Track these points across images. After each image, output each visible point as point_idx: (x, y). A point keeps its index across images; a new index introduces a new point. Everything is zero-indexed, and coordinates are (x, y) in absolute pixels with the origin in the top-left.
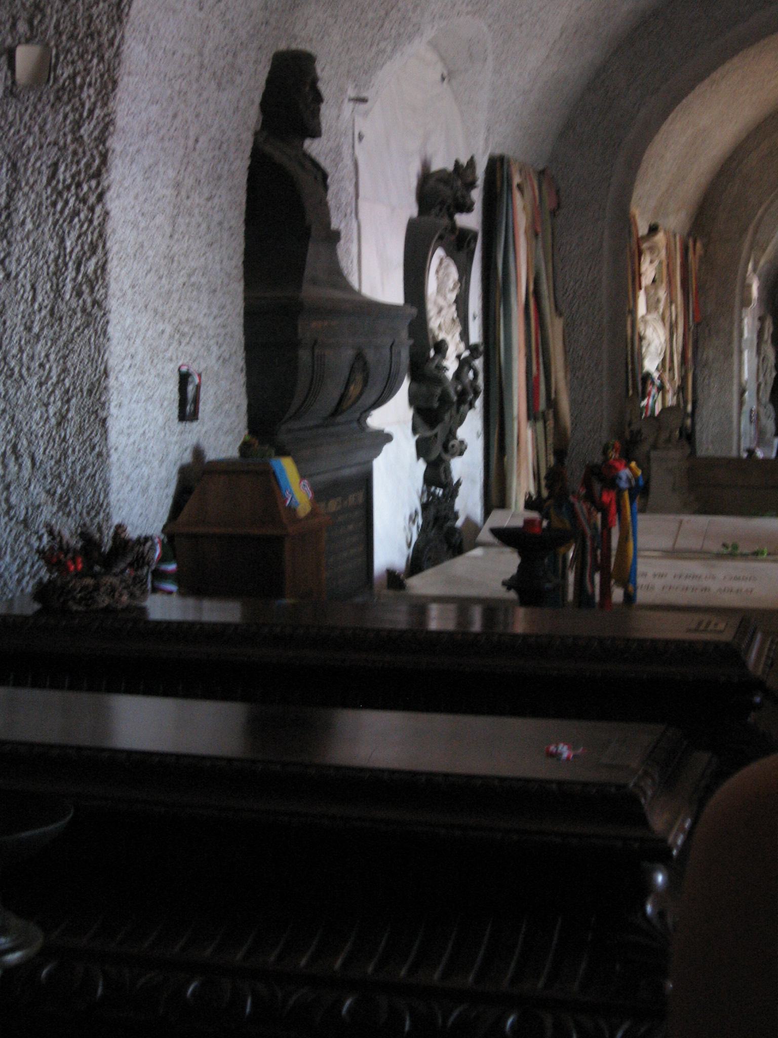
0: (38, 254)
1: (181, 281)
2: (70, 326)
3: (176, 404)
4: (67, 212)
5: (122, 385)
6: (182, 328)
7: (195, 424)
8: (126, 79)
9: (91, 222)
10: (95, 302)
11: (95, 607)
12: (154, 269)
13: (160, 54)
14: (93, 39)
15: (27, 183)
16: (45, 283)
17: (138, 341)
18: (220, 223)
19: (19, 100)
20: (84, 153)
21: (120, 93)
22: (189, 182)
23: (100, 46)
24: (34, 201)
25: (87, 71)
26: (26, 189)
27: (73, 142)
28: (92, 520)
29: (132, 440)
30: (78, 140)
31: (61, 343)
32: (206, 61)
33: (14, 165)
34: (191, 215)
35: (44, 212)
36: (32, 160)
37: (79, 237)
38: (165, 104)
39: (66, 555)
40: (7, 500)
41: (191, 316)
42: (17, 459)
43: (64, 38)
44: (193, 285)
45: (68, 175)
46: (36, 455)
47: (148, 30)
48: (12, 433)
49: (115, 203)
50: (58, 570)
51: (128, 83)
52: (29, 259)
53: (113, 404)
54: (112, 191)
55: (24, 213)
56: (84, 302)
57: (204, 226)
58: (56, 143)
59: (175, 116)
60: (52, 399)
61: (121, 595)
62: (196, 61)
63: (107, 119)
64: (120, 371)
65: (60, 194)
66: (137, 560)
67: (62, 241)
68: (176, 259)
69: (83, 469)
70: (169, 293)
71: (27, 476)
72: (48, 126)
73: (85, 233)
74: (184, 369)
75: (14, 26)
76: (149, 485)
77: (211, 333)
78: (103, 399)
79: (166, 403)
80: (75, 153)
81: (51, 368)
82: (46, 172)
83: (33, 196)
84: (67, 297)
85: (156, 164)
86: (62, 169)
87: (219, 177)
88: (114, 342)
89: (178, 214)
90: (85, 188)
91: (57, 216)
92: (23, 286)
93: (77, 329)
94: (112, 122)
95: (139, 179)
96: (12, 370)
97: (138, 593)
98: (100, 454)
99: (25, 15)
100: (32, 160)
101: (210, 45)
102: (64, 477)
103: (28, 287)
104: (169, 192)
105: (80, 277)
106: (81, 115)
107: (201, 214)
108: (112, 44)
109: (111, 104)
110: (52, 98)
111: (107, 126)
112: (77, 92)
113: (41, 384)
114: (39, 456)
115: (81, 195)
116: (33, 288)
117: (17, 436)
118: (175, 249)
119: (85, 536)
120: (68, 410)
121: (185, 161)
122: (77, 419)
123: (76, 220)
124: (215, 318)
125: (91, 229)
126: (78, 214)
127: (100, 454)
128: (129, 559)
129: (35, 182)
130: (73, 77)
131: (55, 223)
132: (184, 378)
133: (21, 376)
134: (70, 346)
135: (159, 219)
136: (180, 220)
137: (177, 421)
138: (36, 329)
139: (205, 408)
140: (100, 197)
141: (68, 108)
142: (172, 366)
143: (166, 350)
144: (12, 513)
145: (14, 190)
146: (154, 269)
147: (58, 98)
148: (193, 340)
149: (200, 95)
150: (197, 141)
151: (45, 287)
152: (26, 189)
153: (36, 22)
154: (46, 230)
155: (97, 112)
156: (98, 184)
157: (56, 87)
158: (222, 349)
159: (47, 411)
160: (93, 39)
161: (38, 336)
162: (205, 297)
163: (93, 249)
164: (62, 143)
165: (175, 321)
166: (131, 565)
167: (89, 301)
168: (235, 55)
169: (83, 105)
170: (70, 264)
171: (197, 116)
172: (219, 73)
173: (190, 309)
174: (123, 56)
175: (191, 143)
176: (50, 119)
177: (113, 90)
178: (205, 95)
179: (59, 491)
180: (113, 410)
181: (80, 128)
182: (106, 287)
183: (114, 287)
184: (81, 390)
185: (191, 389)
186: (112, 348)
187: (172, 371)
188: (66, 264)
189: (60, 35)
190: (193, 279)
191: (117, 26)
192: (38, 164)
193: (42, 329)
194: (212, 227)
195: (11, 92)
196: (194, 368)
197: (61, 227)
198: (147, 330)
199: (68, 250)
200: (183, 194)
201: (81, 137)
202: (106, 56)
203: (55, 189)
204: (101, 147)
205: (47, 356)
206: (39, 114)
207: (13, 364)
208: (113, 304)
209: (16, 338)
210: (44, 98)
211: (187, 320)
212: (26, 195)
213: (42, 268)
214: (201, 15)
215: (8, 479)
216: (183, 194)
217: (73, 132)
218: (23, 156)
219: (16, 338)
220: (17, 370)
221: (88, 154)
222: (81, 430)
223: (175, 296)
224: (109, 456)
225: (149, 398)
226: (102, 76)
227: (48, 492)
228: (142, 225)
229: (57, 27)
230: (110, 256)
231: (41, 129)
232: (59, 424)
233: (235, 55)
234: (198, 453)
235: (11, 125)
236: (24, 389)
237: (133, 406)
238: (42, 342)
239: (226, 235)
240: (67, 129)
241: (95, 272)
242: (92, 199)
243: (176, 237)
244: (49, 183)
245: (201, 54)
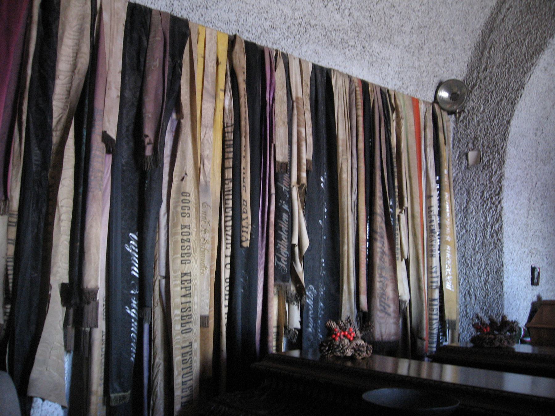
0: (477, 223)
1: (532, 234)
2: (489, 248)
3: (530, 279)
4: (487, 207)
5: (509, 270)
6: (532, 251)
7: (538, 287)
8: (508, 160)
9: (496, 211)
10: (498, 240)
11: (493, 346)
12: (521, 229)
13: (521, 151)
14: (495, 147)
15: (473, 199)
16: (480, 233)
17: (515, 255)
18: (547, 214)
19: (470, 170)
20: (493, 187)
21: (506, 165)
22: (534, 198)
23: (498, 149)
24: (476, 205)
25: (494, 158)
26: (473, 201)
27: (489, 183)
28: (497, 319)
29: (512, 291)
30: (491, 182)
31: (486, 254)
32: (539, 155)
33: (469, 193)
34: (535, 210)
35: (479, 208)
36: (475, 190)
37: (492, 216)
38: (523, 170)
39: (483, 326)
40: (466, 311)
41: (536, 247)
42: (470, 296)
43: (485, 147)
44: (536, 236)
45: (488, 195)
46: (477, 295)
47: (516, 143)
48: (468, 286)
49: (504, 204)
50: (480, 331)
51: (509, 162)
52: (474, 225)
53: (505, 277)
54: (504, 199)
55: (472, 209)
56: (494, 240)
57: (540, 215)
58: (483, 184)
59: (527, 174)
60: (483, 275)
61: (504, 342)
62: (535, 155)
63: (501, 175)
64: (508, 265)
65: (485, 202)
66: (511, 329)
67: (486, 218)
68: (529, 226)
69: (494, 301)
70: (527, 238)
71: (473, 302)
72: (480, 178)
73: (494, 215)
74: (533, 266)
75: (467, 145)
76: (519, 308)
77: (544, 254)
78: (501, 274)
79: (526, 278)
80: (490, 187)
81: (482, 264)
82: (480, 194)
83: (475, 203)
84: (488, 238)
85: (521, 191)
86: (486, 193)
87: (546, 197)
88: (505, 254)
89: (530, 210)
90: (494, 199)
91: (484, 209)
92: (472, 234)
93: (492, 249)
94: (503, 175)
95: (514, 195)
96: (468, 264)
97: (511, 342)
98: (500, 295)
99: (471, 141)
100: (475, 190)
101: (540, 149)
102: (487, 303)
103: (474, 235)
104: (526, 202)
105: (493, 231)
106: (492, 174)
107: (539, 210)
108: (502, 148)
109: (503, 169)
110: (481, 168)
111: (501, 177)
112: (490, 166)
113: (478, 269)
114: (478, 295)
115: (493, 202)
116: (476, 235)
117: (470, 288)
118: (529, 222)
119: (491, 319)
120: (488, 279)
121: (532, 191)
122: (492, 282)
123: (491, 210)
124: (545, 248)
125: (496, 213)
126: (492, 208)
127: (500, 295)
128: (508, 328)
129: (476, 198)
130: (489, 161)
131: (483, 212)
132: (533, 269)
133: (471, 266)
134: (489, 256)
135: (522, 211)
136: (531, 212)
137: (530, 285)
138: (477, 250)
139: (542, 281)
140: (499, 202)
141: (487, 172)
142: (528, 265)
143: (526, 259)
144: (468, 316)
145: (468, 201)
146: (521, 229)
147: (484, 169)
148: (537, 256)
149: (537, 167)
150: (536, 184)
151: (479, 235)
152: (473, 201)
153: (475, 143)
154: (480, 215)
155: (498, 172)
156: (499, 198)
157: (483, 165)
158: (549, 260)
159: (481, 279)
160: (495, 147)
161: (477, 252)
162: (541, 240)
163: (497, 220)
164: (485, 184)
165: (530, 248)
166: (508, 331)
167: (496, 239)
168: (550, 153)
169: (492, 170)
170: (489, 226)
171: (536, 174)
172: (544, 159)
173: (535, 244)
174: (507, 152)
175: (534, 184)
176: (481, 176)
177: (503, 164)
178: (539, 167)
179: (485, 308)
180: (505, 279)
181: (491, 178)
182: (502, 234)
183: (505, 234)
184: (493, 271)
185: (536, 273)
186: (505, 256)
187: (529, 266)
188: (487, 226)
189: (484, 147)
190: (536, 234)
191: (504, 142)
192: (477, 192)
193: (479, 250)
194: (543, 215)
195: (467, 168)
196: (537, 266)
197: (486, 213)
198: (519, 251)
199: (488, 221)
200: (532, 202)
201: (492, 181)
202: (500, 153)
203: (483, 200)
204: (499, 184)
205: (481, 259)
206: (477, 174)
207: (468, 262)
208: (505, 240)
209: (469, 253)
210: (479, 169)
211: (534, 248)
212: (473, 203)
213: (479, 228)
214: (536, 138)
215: (466, 303)
216: (532, 202)
217: (489, 180)
218: (472, 189)
219: (469, 253)
220: (470, 264)
221: (495, 187)
222: (493, 286)
223: (530, 239)
224: (503, 295)
225: (519, 276)
226: (499, 160)
227: (481, 308)
228: (516, 212)
229: (482, 144)
230: (503, 223)
231: (478, 180)
232: (485, 284)
233: (550, 153)
234: (539, 298)
235: (467, 179)
236: (472, 271)
237: (513, 278)
238: (479, 254)
239: (549, 218)
240: (487, 179)
241: (498, 229)
242: (497, 203)
243: (529, 218)
244: (481, 198)
245: (537, 152)
